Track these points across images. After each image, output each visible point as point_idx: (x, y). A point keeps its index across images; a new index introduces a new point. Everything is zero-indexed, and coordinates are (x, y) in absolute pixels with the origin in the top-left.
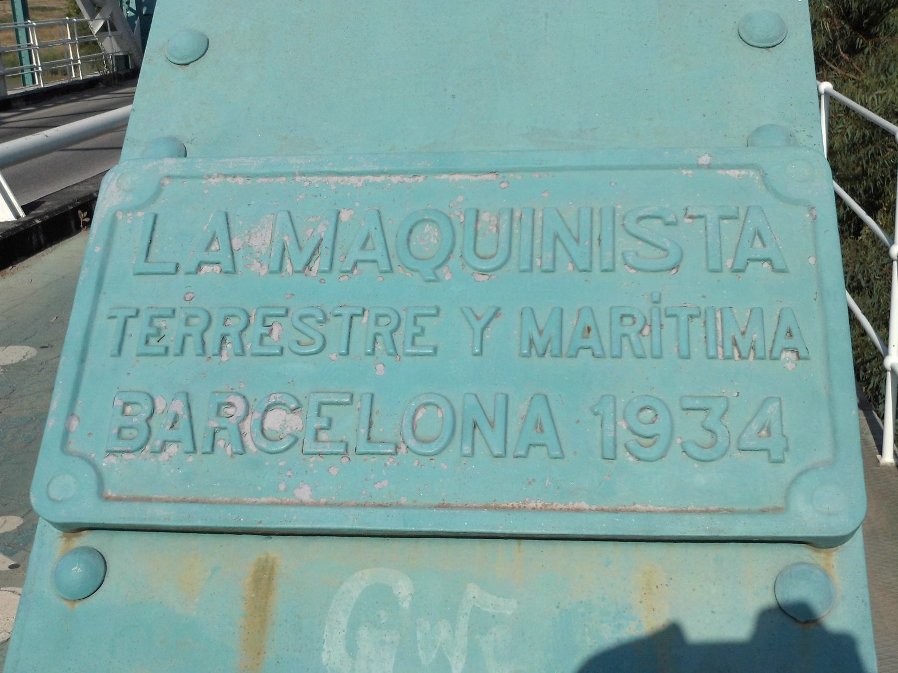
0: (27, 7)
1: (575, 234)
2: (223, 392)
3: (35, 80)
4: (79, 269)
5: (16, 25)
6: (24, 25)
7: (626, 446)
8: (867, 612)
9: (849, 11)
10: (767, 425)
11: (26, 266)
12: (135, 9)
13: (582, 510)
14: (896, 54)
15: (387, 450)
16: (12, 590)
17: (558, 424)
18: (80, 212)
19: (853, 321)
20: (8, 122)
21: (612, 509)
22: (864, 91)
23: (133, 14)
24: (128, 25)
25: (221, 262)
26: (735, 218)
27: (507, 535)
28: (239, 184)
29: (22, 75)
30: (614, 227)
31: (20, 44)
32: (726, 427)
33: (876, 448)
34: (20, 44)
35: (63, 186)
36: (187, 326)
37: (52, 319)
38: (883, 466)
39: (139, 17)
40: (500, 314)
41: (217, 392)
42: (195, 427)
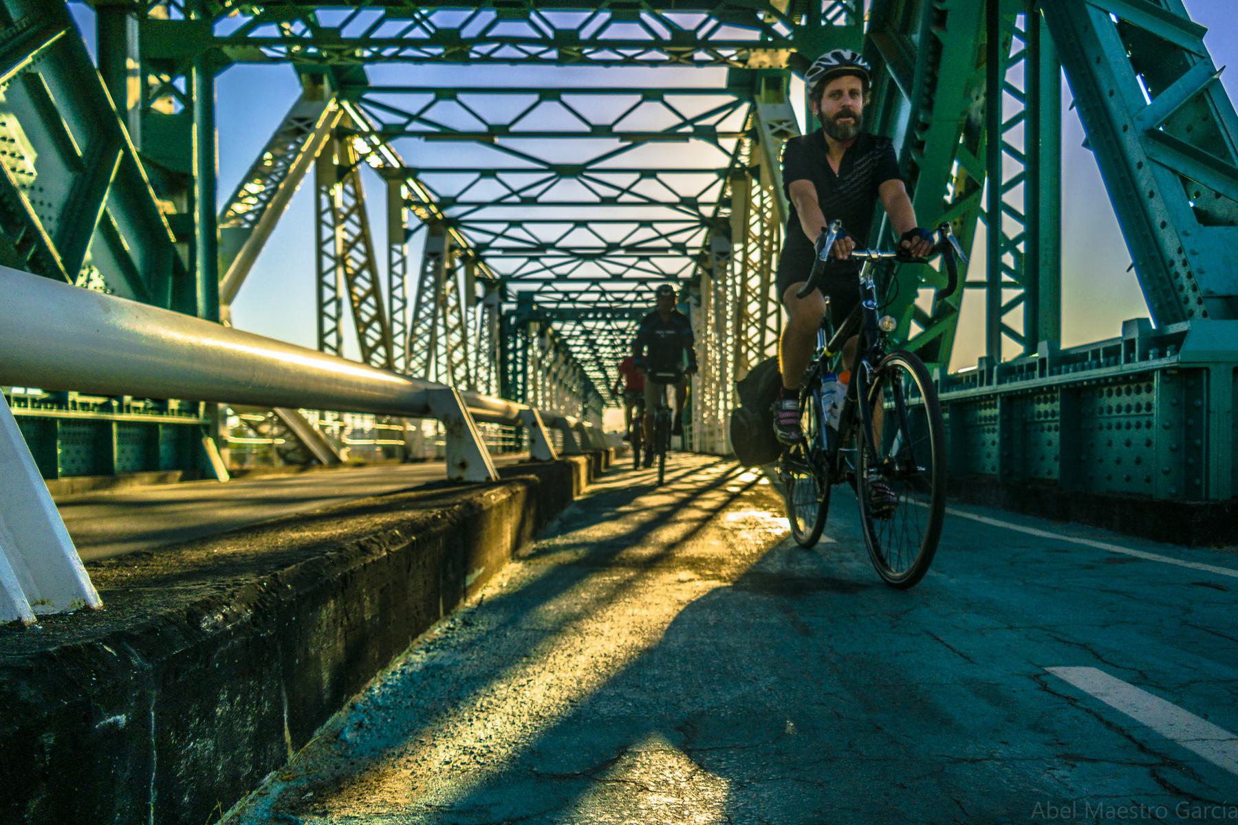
2: (1094, 653)
6: (501, 443)
9: (585, 400)
12: (1023, 30)
13: (688, 563)
14: (346, 426)
16: (1181, 169)
20: (790, 418)
22: (352, 578)
24: (685, 427)
34: (1035, 363)
35: (1177, 41)
37: (534, 481)
38: (722, 773)
39: (63, 33)
40: (978, 65)
42: (636, 234)
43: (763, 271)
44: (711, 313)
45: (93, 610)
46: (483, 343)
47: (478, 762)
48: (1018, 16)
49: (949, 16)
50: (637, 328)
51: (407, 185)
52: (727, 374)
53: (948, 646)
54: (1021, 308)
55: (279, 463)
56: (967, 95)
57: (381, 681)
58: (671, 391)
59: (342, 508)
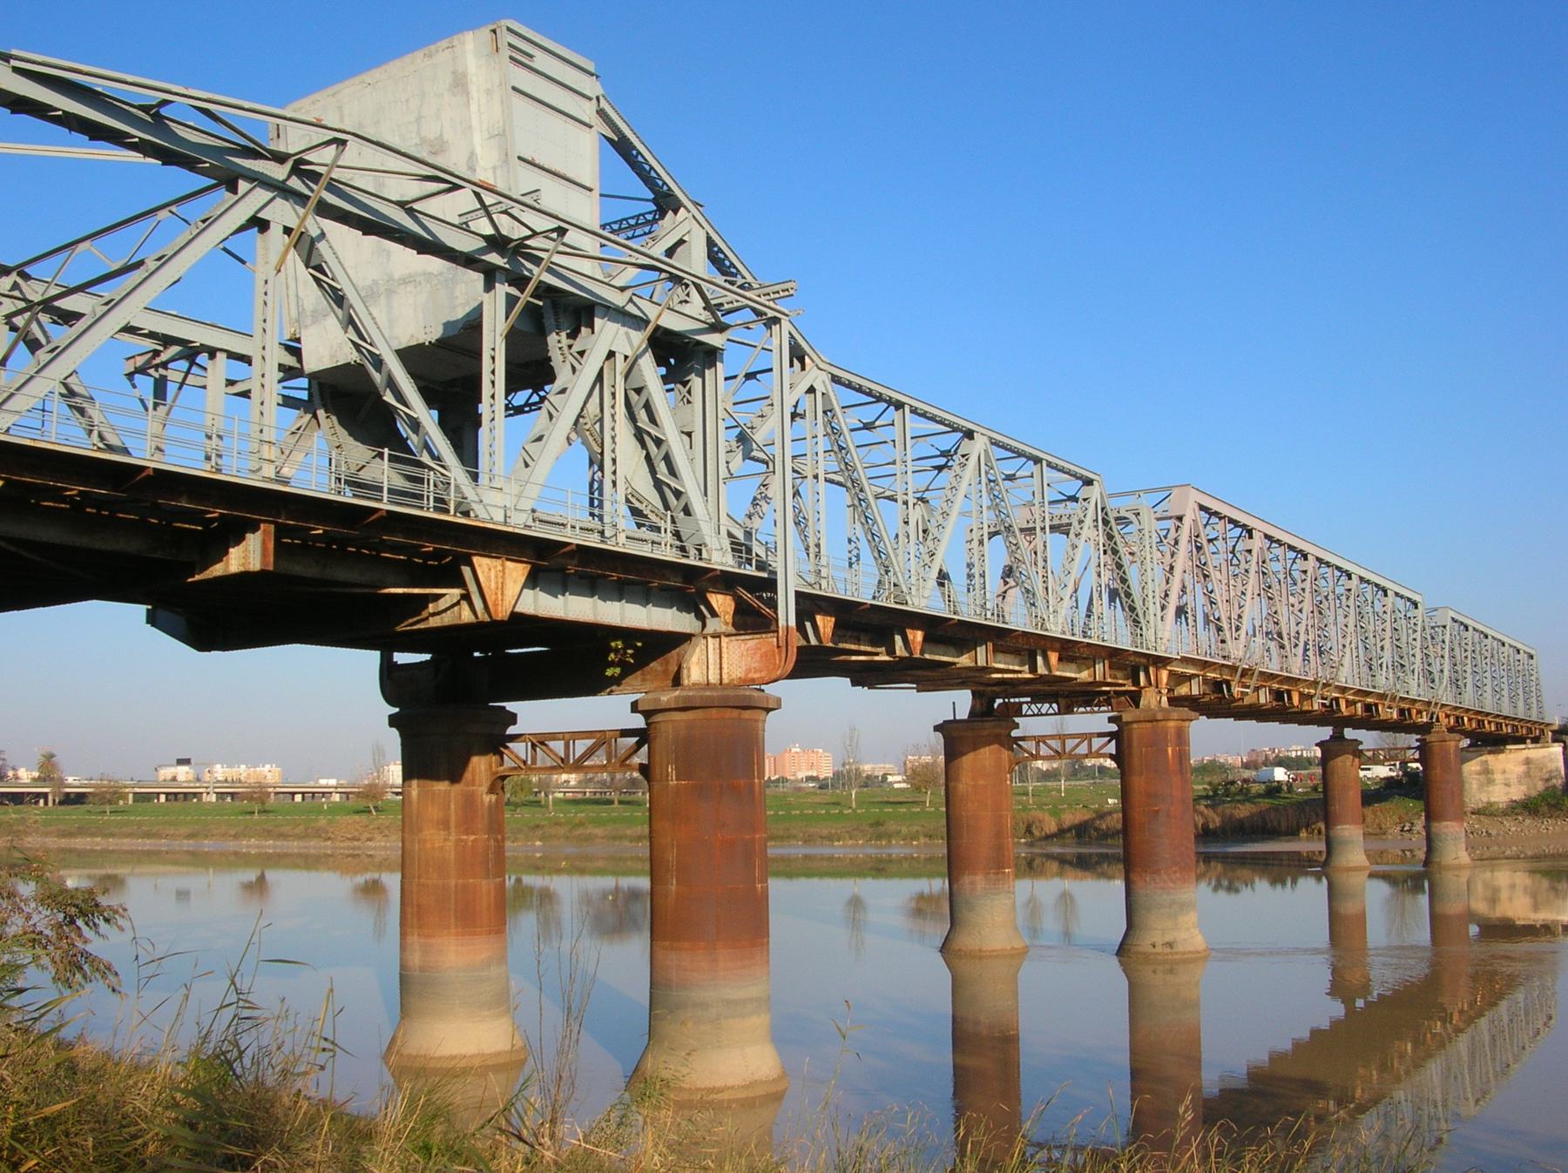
0: (618, 875)
1: (930, 488)
3: (620, 591)
4: (1364, 909)
5: (1043, 529)
7: (500, 203)
8: (482, 29)
10: (1071, 850)
11: (1081, 515)
15: (194, 577)
17: (348, 270)
18: (1197, 807)
19: (126, 451)
21: (430, 342)
23: (819, 618)
25: (55, 752)
26: (660, 305)
27: (272, 182)
28: (664, 373)
29: (1034, 528)
30: (901, 803)
31: (1051, 532)
32: (153, 945)
33: (409, 1065)
36: (1363, 797)
41: (1084, 658)
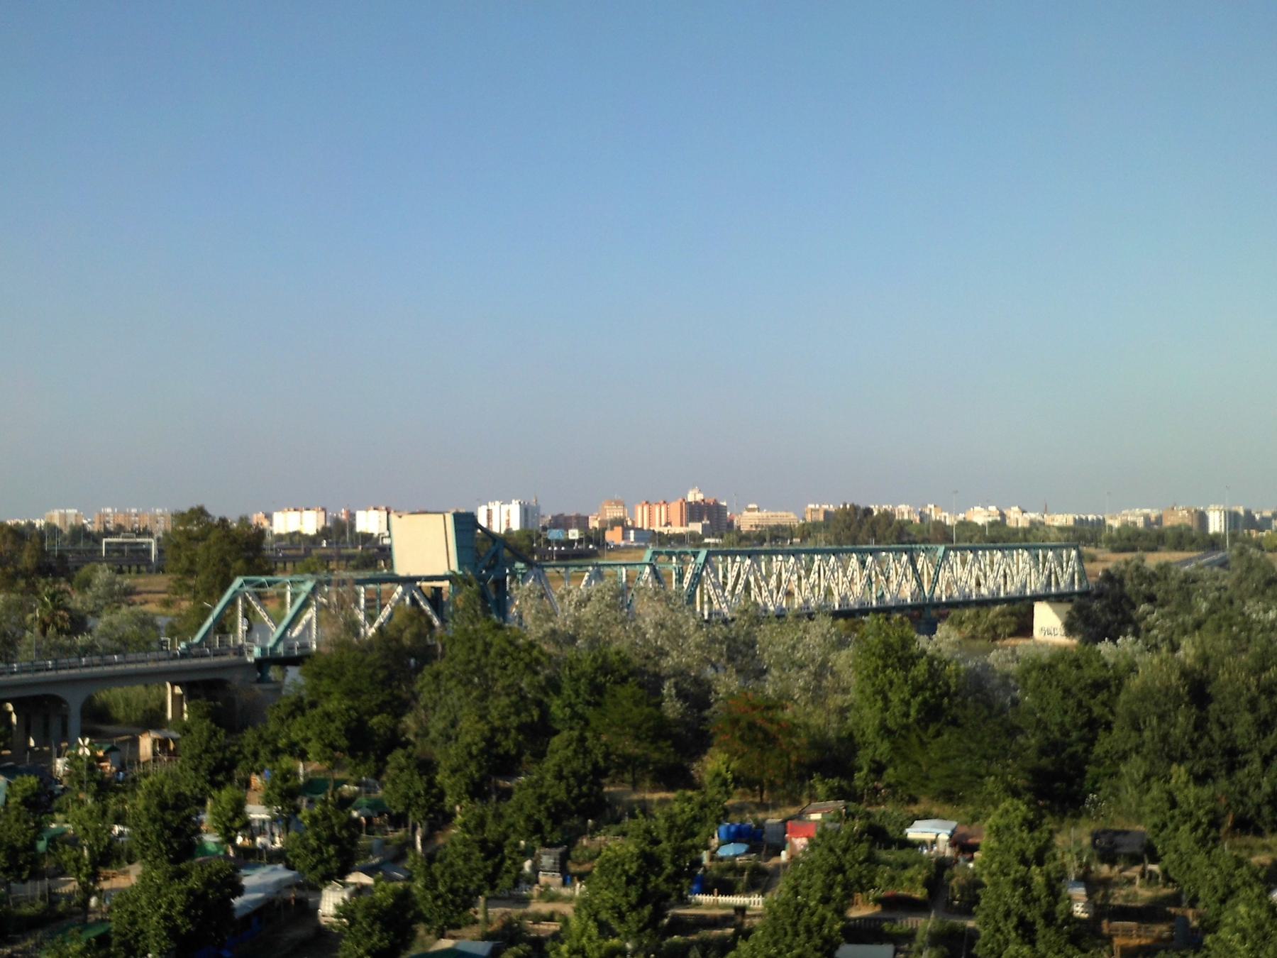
43: (567, 567)
44: (1153, 560)
45: (314, 540)
46: (831, 717)
47: (565, 619)
48: (409, 643)
49: (462, 510)
50: (37, 526)
51: (932, 590)
52: (696, 933)
53: (635, 564)
54: (529, 719)
55: (1265, 908)
56: (617, 503)
57: (733, 620)
58: (756, 506)
59: (1156, 897)
